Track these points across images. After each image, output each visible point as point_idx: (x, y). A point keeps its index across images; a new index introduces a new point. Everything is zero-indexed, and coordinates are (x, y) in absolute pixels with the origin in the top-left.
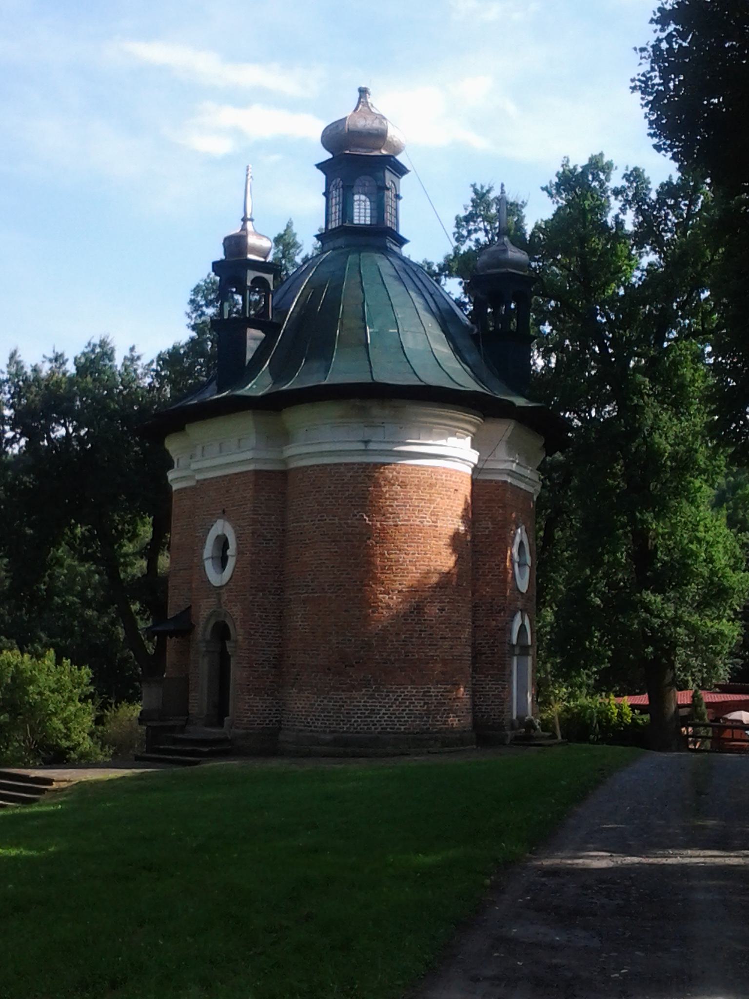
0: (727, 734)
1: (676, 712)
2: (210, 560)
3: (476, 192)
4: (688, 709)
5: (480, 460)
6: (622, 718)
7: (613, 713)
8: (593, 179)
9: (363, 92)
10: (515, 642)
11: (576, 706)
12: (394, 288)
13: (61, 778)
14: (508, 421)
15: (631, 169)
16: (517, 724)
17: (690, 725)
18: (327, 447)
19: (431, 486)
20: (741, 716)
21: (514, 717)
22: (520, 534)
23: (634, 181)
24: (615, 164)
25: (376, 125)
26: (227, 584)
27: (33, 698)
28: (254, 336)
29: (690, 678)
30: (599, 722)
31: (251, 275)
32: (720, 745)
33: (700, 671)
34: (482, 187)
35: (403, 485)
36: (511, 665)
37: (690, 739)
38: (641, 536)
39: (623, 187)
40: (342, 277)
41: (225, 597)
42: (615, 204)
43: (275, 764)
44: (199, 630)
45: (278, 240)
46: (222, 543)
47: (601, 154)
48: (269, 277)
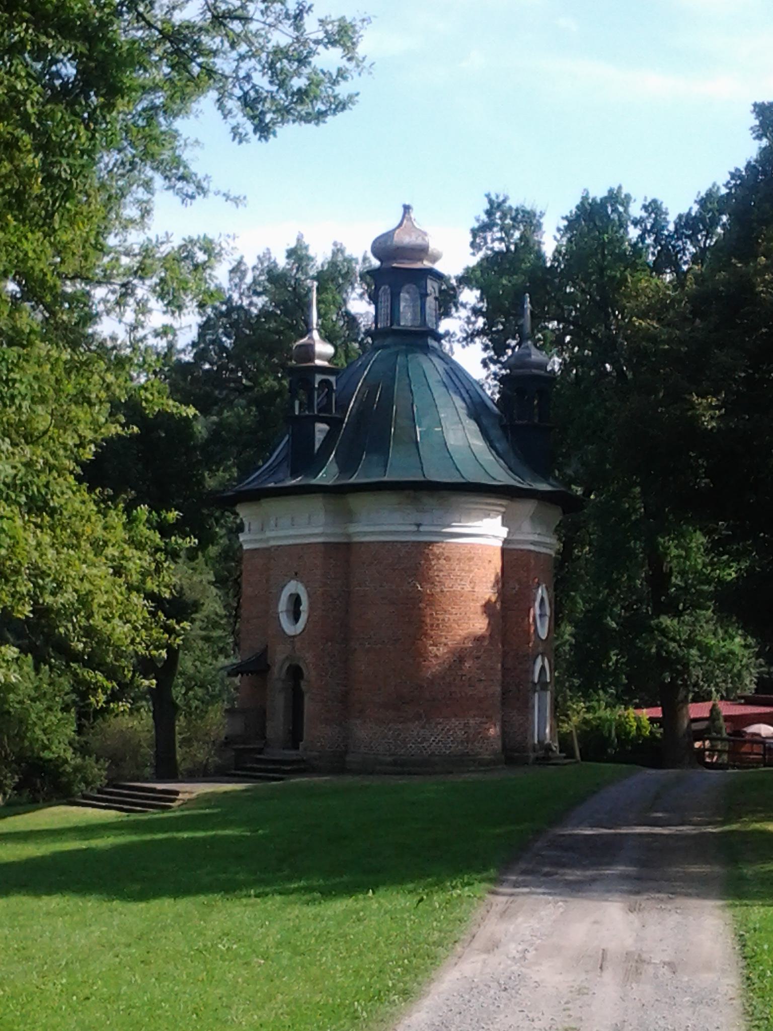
0: (746, 748)
1: (689, 726)
2: (285, 614)
3: (491, 202)
4: (706, 723)
5: (509, 533)
6: (640, 731)
7: (631, 726)
8: (613, 211)
9: (407, 208)
10: (536, 680)
11: (594, 718)
12: (438, 391)
13: (184, 790)
14: (533, 501)
15: (649, 200)
16: (538, 747)
17: (707, 739)
18: (385, 528)
19: (471, 559)
20: (760, 729)
21: (536, 742)
22: (541, 592)
23: (652, 212)
24: (633, 196)
25: (419, 241)
26: (300, 634)
27: (13, 707)
28: (321, 428)
29: (713, 689)
30: (618, 736)
31: (319, 378)
32: (737, 759)
33: (724, 681)
34: (497, 197)
35: (448, 559)
36: (533, 698)
37: (707, 753)
38: (656, 558)
39: (641, 217)
40: (393, 379)
41: (298, 645)
42: (634, 233)
43: (349, 780)
44: (275, 670)
45: (291, 253)
46: (296, 600)
47: (620, 188)
48: (332, 379)
